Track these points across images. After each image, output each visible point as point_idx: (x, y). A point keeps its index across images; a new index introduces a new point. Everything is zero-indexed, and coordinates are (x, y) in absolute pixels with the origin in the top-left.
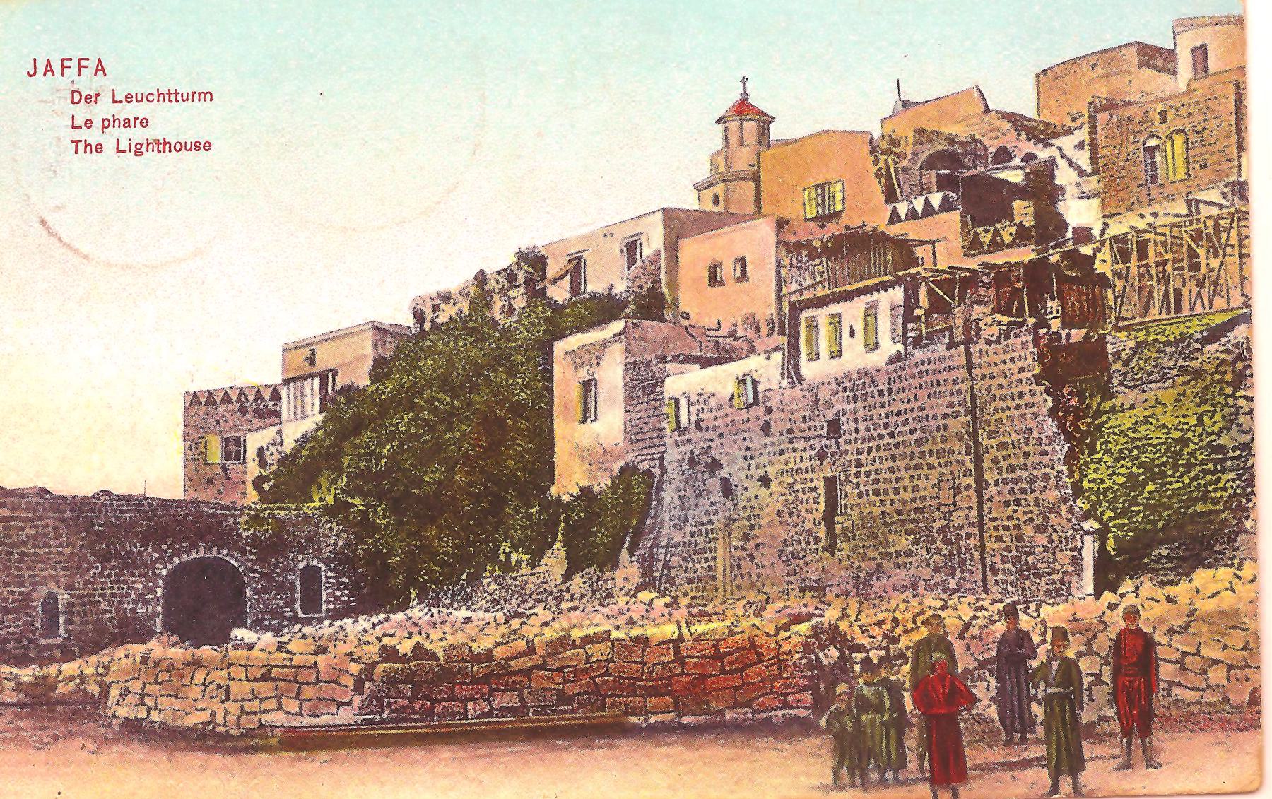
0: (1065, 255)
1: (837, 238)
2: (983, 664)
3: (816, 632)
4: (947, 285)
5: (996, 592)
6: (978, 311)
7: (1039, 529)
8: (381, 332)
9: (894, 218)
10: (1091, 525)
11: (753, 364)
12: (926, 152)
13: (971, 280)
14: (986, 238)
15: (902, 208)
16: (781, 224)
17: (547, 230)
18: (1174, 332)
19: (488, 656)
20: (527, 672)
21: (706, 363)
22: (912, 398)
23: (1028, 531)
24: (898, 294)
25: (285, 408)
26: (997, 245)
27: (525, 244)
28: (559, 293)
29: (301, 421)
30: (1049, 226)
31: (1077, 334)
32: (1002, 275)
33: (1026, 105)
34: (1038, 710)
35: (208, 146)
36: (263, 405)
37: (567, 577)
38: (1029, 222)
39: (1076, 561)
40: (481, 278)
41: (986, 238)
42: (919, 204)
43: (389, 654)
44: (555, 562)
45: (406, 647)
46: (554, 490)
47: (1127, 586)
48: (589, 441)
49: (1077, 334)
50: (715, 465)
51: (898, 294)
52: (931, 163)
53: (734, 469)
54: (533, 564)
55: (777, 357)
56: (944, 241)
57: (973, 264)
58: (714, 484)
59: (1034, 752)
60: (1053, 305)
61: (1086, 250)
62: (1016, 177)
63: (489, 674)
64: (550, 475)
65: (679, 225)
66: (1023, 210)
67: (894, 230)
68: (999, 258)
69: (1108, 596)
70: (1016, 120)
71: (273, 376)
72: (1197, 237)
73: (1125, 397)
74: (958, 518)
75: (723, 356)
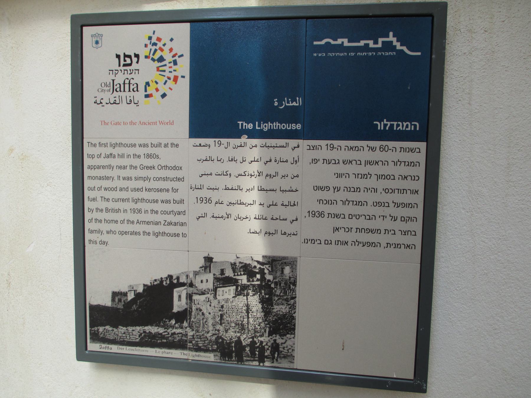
0: (265, 283)
1: (224, 278)
2: (247, 345)
3: (218, 336)
4: (244, 287)
5: (250, 334)
6: (249, 291)
7: (259, 326)
8: (144, 285)
9: (235, 275)
10: (268, 326)
11: (208, 295)
12: (241, 265)
13: (248, 286)
14: (251, 280)
15: (236, 274)
16: (214, 275)
17: (174, 273)
18: (285, 297)
19: (161, 334)
20: (168, 337)
21: (200, 295)
22: (205, 281)
23: (257, 326)
24: (235, 287)
25: (128, 295)
26: (253, 281)
27: (170, 274)
28: (175, 281)
29: (131, 296)
30: (263, 278)
31: (267, 296)
32: (254, 286)
33: (261, 260)
34: (257, 353)
35: (177, 146)
36: (125, 294)
37: (175, 324)
38: (259, 278)
39: (265, 331)
40: (162, 278)
41: (251, 280)
42: (239, 274)
43: (145, 332)
44: (173, 322)
45: (148, 332)
46: (173, 311)
47: (274, 335)
48: (179, 304)
49: (267, 296)
50: (201, 310)
51: (235, 287)
52: (241, 267)
53: (204, 311)
54: (169, 321)
55: (212, 295)
56: (243, 279)
57: (249, 283)
58: (201, 313)
59: (256, 359)
60: (263, 291)
61: (270, 283)
62: (257, 271)
63: (161, 336)
64: (172, 308)
65: (196, 273)
66: (258, 276)
67: (234, 277)
68: (253, 283)
69: (270, 337)
70: (258, 262)
71: (127, 290)
72: (290, 283)
73: (275, 307)
74: (244, 322)
75: (203, 294)
